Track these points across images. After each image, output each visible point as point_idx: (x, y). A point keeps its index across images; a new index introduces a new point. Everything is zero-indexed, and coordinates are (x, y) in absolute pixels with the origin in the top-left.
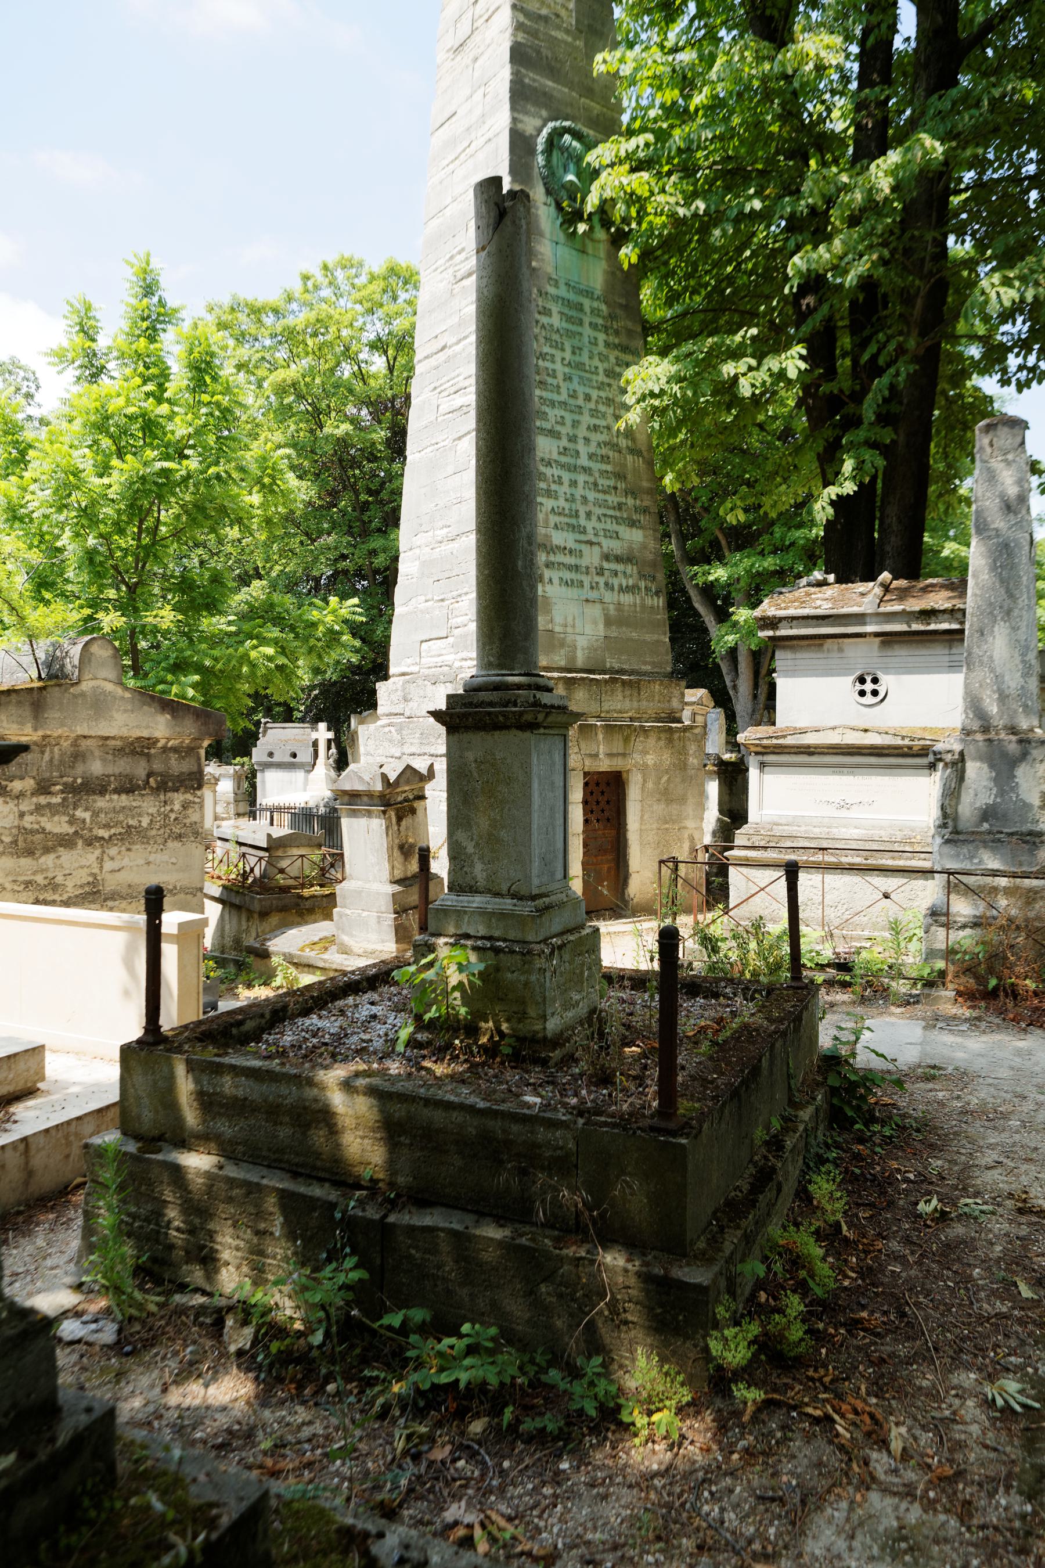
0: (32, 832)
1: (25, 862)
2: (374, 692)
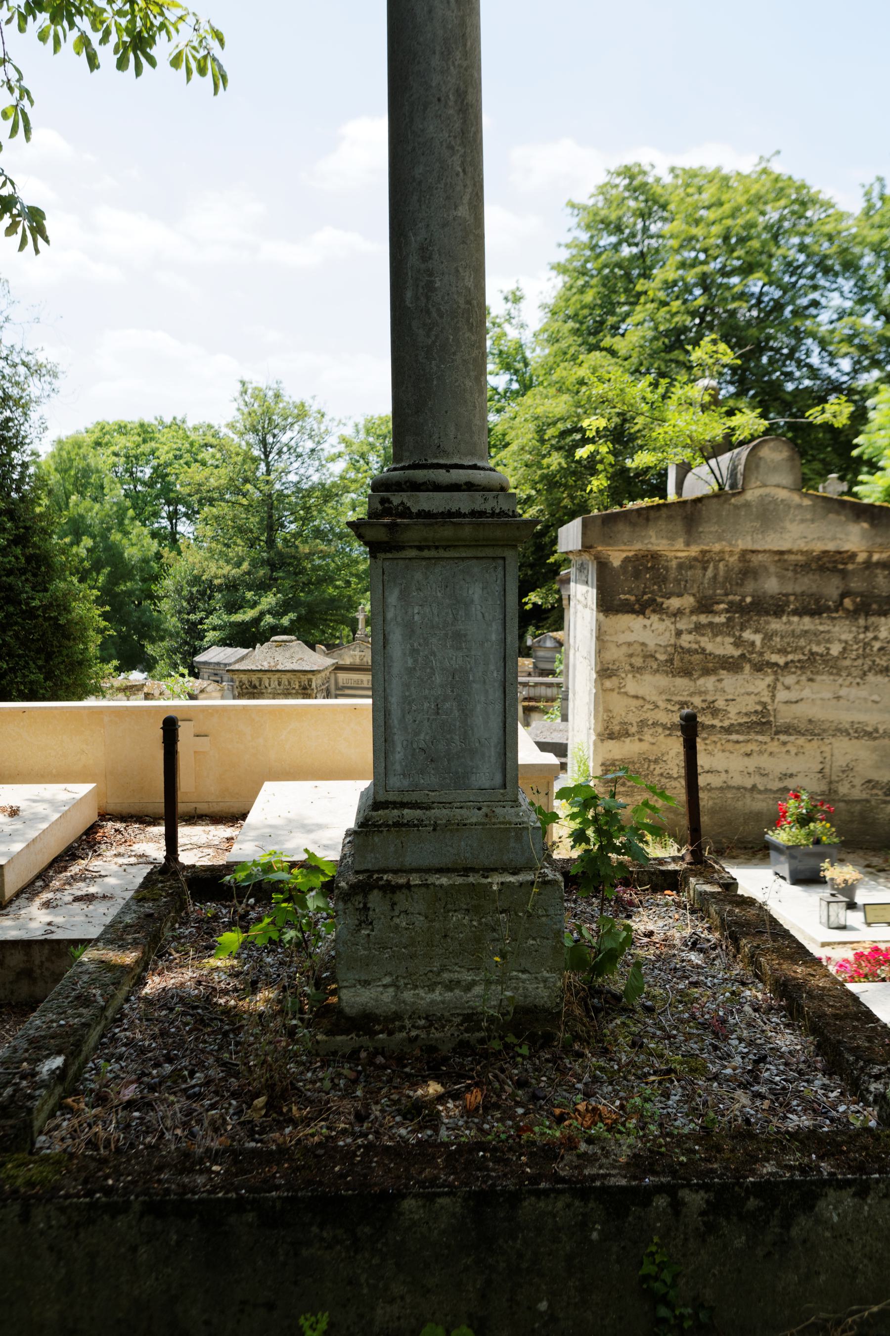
0: (689, 651)
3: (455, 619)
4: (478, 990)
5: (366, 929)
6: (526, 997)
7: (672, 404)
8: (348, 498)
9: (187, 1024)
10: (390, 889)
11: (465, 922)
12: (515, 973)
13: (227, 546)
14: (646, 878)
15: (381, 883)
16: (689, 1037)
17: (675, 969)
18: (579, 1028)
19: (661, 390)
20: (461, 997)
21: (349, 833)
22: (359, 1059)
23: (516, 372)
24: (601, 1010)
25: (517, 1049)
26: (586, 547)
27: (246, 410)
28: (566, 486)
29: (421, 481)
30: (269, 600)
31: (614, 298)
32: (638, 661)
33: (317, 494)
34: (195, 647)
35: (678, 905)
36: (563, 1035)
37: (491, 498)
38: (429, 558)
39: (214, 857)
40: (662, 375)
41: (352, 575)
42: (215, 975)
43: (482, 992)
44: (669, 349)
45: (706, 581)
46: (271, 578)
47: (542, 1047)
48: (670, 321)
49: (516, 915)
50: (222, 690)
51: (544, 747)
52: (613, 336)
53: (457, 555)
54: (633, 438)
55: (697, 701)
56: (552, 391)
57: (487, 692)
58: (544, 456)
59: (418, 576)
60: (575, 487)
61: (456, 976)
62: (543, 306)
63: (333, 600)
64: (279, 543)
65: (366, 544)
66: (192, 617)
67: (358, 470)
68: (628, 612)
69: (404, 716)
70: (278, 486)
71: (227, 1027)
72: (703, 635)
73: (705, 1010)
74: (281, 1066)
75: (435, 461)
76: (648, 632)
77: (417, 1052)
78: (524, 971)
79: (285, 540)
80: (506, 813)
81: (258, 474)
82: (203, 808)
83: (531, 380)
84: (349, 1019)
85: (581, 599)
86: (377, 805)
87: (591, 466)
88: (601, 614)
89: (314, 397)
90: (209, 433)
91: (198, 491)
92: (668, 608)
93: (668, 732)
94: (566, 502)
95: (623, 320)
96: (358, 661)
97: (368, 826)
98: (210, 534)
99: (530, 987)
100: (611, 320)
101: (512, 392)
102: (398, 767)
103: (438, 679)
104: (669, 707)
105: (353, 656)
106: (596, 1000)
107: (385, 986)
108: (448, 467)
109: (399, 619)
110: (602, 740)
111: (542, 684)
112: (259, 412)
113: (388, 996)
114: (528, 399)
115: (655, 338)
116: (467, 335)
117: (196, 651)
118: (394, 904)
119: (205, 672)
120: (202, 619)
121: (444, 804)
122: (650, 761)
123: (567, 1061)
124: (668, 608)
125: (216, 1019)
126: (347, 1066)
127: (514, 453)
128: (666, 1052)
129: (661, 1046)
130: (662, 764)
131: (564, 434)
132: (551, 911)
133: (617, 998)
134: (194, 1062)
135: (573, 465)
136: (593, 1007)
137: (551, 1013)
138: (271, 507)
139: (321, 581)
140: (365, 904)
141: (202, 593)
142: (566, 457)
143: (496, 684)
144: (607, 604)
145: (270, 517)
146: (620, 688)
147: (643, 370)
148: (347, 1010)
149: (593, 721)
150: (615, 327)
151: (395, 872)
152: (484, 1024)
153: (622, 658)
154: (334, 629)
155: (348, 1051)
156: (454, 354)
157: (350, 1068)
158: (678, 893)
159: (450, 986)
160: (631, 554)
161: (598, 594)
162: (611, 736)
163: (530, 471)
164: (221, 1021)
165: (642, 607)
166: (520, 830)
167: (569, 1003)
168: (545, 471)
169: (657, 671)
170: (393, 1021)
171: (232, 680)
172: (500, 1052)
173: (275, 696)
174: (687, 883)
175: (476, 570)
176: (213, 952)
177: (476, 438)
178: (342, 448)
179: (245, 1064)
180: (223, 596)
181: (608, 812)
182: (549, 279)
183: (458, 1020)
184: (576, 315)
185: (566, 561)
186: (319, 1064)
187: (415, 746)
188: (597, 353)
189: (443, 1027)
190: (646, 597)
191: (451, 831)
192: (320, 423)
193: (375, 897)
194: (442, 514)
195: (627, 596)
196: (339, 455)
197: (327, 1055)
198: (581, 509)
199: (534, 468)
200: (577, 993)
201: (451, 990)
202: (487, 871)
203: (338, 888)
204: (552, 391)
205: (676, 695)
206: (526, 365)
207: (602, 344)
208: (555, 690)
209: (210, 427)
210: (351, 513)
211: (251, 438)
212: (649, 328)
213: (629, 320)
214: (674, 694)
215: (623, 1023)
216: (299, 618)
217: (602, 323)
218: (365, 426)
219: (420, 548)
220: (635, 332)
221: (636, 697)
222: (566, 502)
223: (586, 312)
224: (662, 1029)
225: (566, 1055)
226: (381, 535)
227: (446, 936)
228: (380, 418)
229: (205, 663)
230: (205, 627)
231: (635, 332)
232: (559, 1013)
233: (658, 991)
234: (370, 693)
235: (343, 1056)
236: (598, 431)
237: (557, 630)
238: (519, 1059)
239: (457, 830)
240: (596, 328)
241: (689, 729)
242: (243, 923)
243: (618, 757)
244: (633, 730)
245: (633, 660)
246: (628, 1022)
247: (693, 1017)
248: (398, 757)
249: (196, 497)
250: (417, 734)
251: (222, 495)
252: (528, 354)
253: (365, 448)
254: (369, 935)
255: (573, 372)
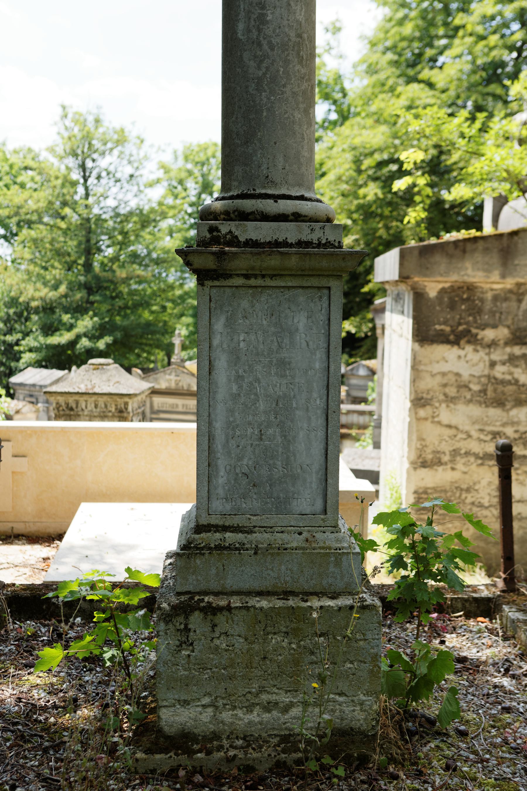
0: (503, 382)
1: (494, 412)
2: (79, 505)
3: (280, 347)
4: (295, 711)
5: (187, 650)
6: (342, 719)
7: (490, 138)
8: (164, 224)
9: (8, 740)
10: (212, 611)
11: (284, 644)
12: (332, 696)
13: (46, 269)
14: (460, 605)
15: (202, 605)
16: (501, 761)
17: (488, 694)
18: (394, 750)
19: (478, 125)
20: (279, 719)
21: (169, 556)
22: (178, 777)
23: (335, 102)
24: (417, 733)
25: (333, 770)
26: (404, 278)
27: (66, 134)
28: (382, 216)
29: (249, 211)
30: (86, 323)
31: (433, 31)
32: (452, 391)
33: (135, 219)
34: (10, 369)
35: (492, 631)
36: (378, 757)
37: (317, 229)
38: (256, 287)
39: (31, 576)
40: (479, 108)
41: (168, 300)
42: (35, 692)
43: (300, 714)
44: (488, 81)
45: (520, 313)
46: (88, 302)
47: (357, 769)
48: (487, 55)
49: (335, 638)
50: (37, 411)
51: (359, 474)
52: (432, 68)
53: (283, 284)
54: (449, 170)
55: (509, 431)
56: (370, 122)
57: (309, 419)
58: (361, 187)
59: (245, 304)
60: (391, 218)
61: (274, 697)
62: (362, 37)
63: (148, 324)
64: (96, 265)
65: (195, 271)
66: (9, 338)
67: (176, 197)
68: (443, 342)
69: (227, 442)
70: (96, 211)
71: (47, 744)
72: (517, 366)
73: (518, 735)
74: (101, 783)
75: (263, 191)
76: (462, 362)
77: (235, 772)
78: (340, 694)
79: (102, 264)
80: (326, 538)
81: (77, 198)
82: (20, 528)
83: (349, 110)
84: (168, 738)
85: (396, 329)
86: (199, 529)
87: (408, 197)
88: (417, 345)
89: (133, 123)
90: (30, 156)
91: (17, 214)
92: (482, 339)
93: (480, 462)
94: (382, 232)
95: (441, 53)
96: (173, 385)
97: (190, 548)
98: (28, 256)
99: (347, 710)
100: (429, 52)
101: (330, 122)
102: (221, 491)
103: (262, 406)
104: (482, 437)
105: (169, 381)
106: (410, 724)
107: (204, 706)
108: (276, 198)
109: (225, 346)
110: (415, 469)
111: (354, 412)
112: (79, 136)
113: (207, 716)
114: (345, 130)
115: (474, 72)
116: (297, 68)
117: (11, 373)
118: (214, 626)
119: (20, 393)
120: (18, 340)
121: (268, 529)
122: (462, 490)
123: (382, 783)
124: (482, 339)
125: (36, 735)
126: (165, 783)
127: (331, 183)
128: (478, 775)
129: (474, 770)
130: (474, 493)
131: (381, 164)
132: (369, 636)
133: (431, 722)
134: (14, 777)
135: (389, 196)
136: (408, 730)
137: (367, 736)
138: (89, 231)
139: (136, 306)
140: (186, 625)
141: (20, 315)
142: (383, 188)
143: (319, 412)
144: (423, 335)
145: (88, 241)
146: (433, 417)
147: (460, 102)
148: (166, 729)
149: (406, 449)
150: (433, 60)
151: (216, 594)
152: (302, 746)
153: (437, 388)
154: (149, 353)
155: (166, 769)
156: (284, 86)
157: (169, 786)
158: (491, 620)
159: (268, 707)
160: (447, 285)
161: (414, 324)
162: (424, 464)
163: (346, 201)
164: (41, 737)
165: (457, 338)
166: (339, 556)
167: (384, 725)
168: (361, 201)
169: (470, 401)
170: (211, 740)
171: (47, 402)
172: (316, 772)
173: (91, 418)
174: (501, 610)
175: (301, 299)
176: (32, 670)
177: (303, 169)
178: (160, 174)
179: (66, 780)
180: (40, 318)
181: (425, 539)
182: (369, 11)
183: (276, 740)
184: (395, 47)
185: (382, 291)
186: (138, 781)
187: (238, 471)
188: (415, 86)
189: (261, 747)
190: (461, 328)
191: (272, 554)
192: (139, 148)
193: (196, 618)
194: (269, 244)
195: (443, 327)
196: (158, 181)
197: (146, 773)
198: (395, 240)
199: (350, 198)
200: (393, 717)
201: (269, 711)
202: (306, 595)
203: (159, 608)
204: (370, 122)
205: (489, 425)
206: (345, 95)
207: (421, 76)
208: (367, 418)
209: (30, 150)
210: (168, 238)
211: (71, 162)
212: (467, 62)
213: (447, 53)
214: (486, 424)
215: (437, 747)
216: (115, 342)
217: (420, 55)
218: (184, 153)
219: (247, 277)
220: (453, 65)
221: (449, 426)
222: (382, 232)
223: (404, 44)
224: (475, 753)
225: (381, 776)
226: (210, 263)
227: (265, 658)
228: (199, 146)
229: (21, 385)
230: (22, 348)
231: (453, 65)
232: (374, 736)
233: (471, 716)
234: (194, 418)
235: (162, 774)
236: (415, 163)
237: (370, 358)
238: (335, 780)
239: (278, 554)
240: (415, 60)
241: (505, 459)
242: (58, 638)
243: (430, 485)
244: (446, 458)
245: (447, 390)
246: (441, 745)
247: (506, 742)
248: (221, 481)
249: (14, 220)
250: (240, 459)
251: (40, 218)
252: (347, 85)
253: (183, 175)
254: (189, 656)
255: (391, 103)
